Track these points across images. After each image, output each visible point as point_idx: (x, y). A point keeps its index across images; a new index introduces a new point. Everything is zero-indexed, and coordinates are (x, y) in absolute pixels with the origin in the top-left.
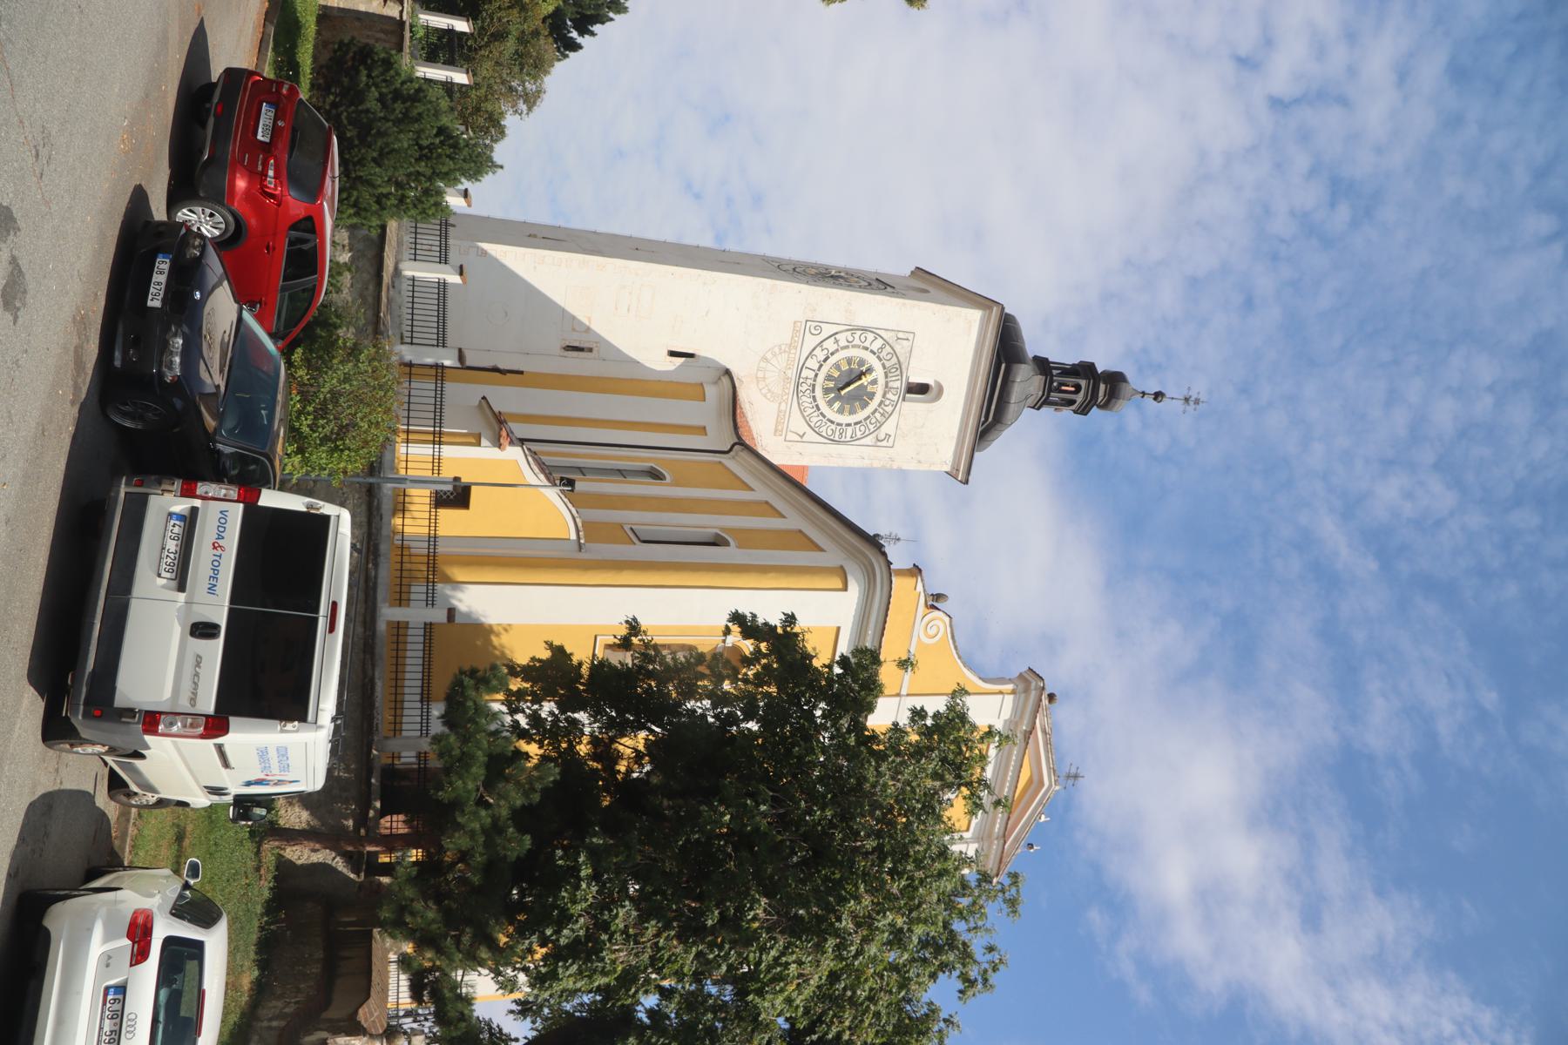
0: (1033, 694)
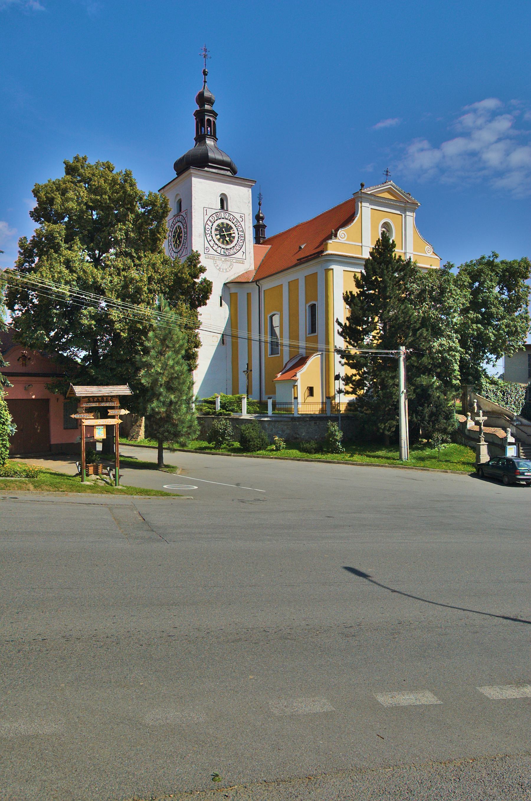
0: (362, 195)
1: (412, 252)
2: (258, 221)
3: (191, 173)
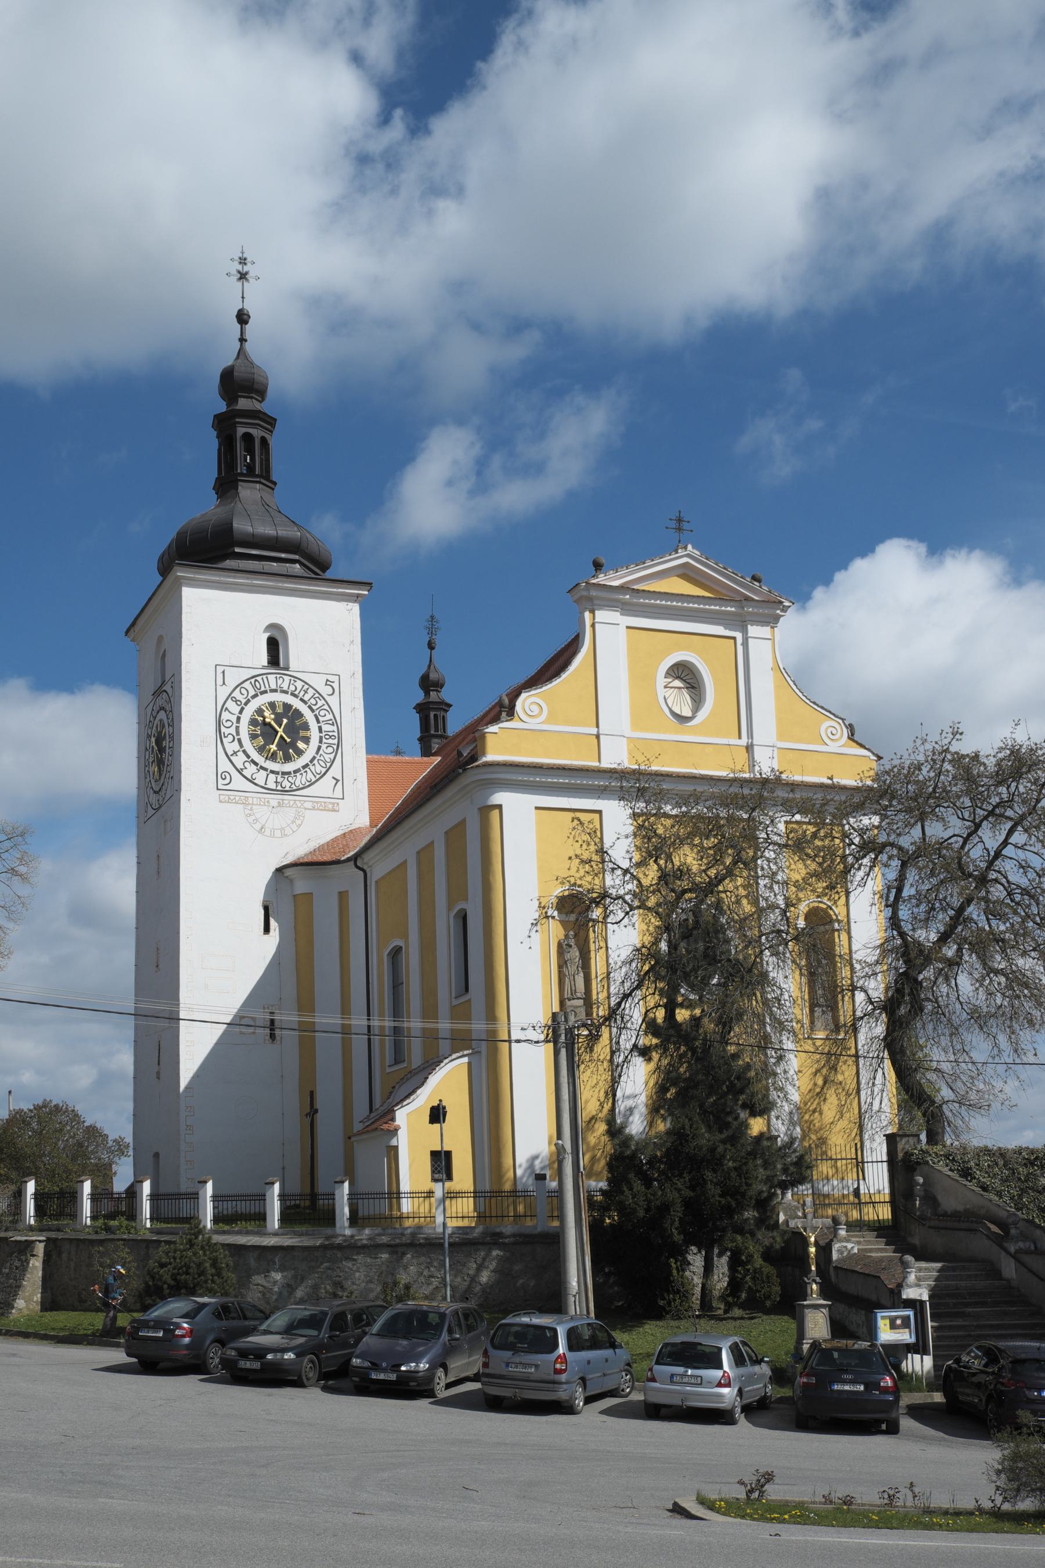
0: (594, 593)
1: (772, 739)
2: (427, 693)
3: (179, 578)
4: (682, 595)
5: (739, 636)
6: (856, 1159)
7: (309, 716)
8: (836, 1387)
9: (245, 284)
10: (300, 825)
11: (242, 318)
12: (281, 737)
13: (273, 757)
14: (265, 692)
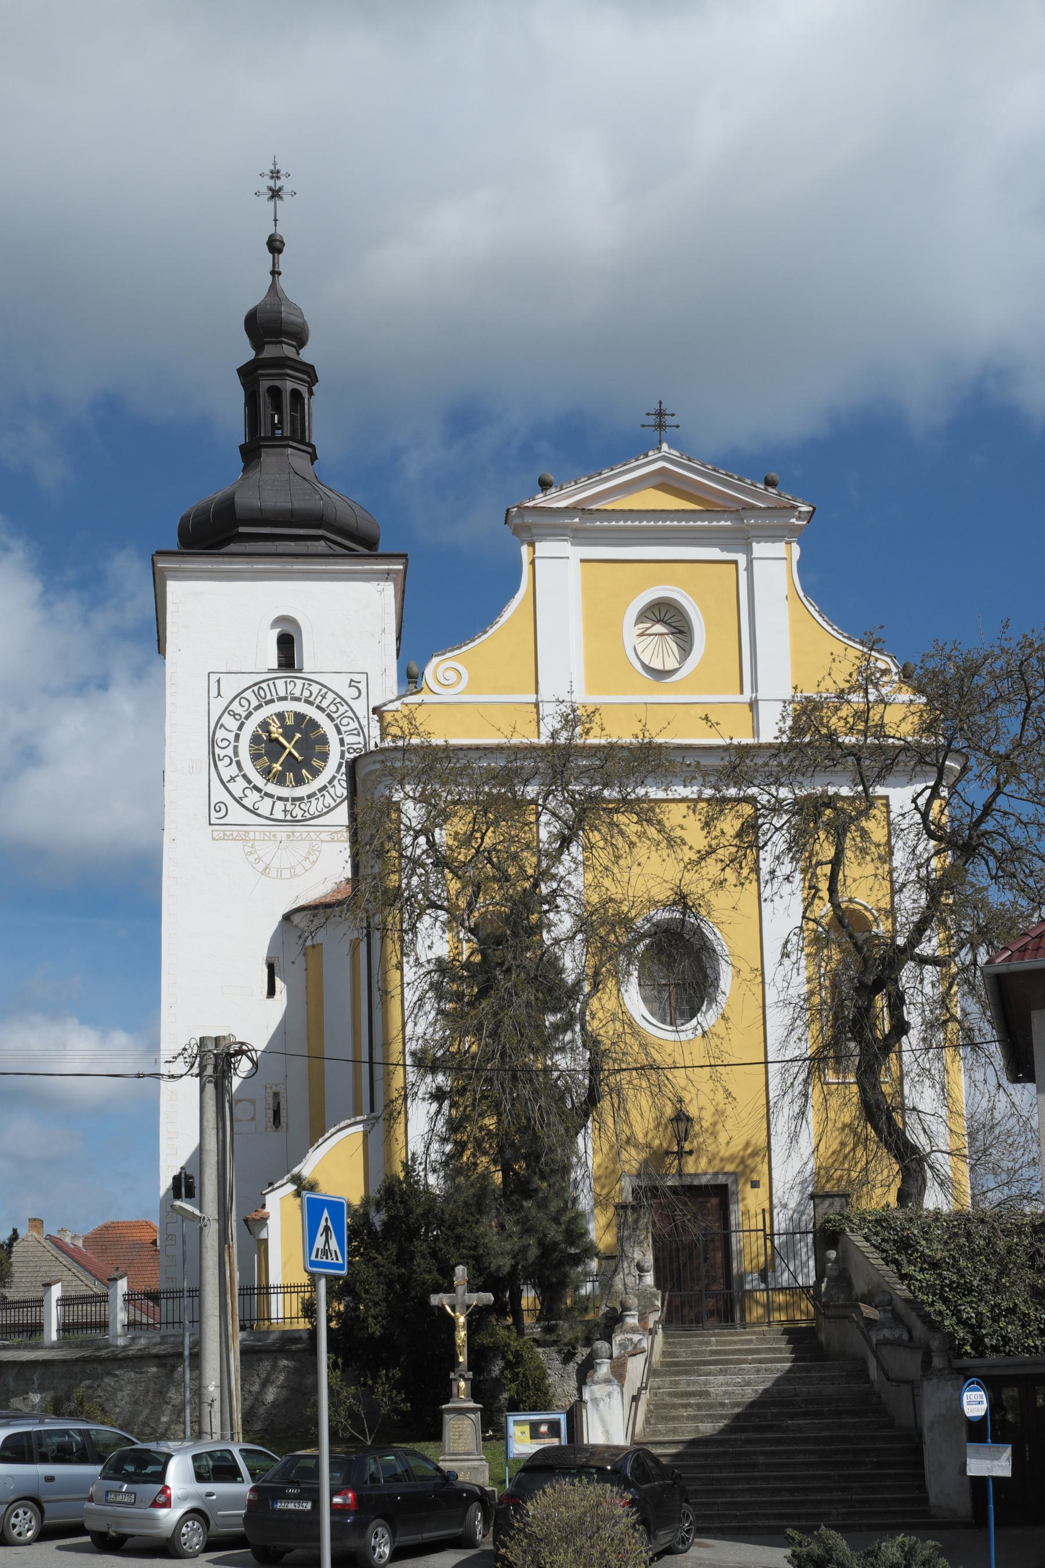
0: (529, 520)
4: (654, 511)
5: (741, 558)
6: (764, 1230)
7: (327, 727)
8: (280, 1505)
9: (279, 202)
10: (315, 862)
11: (275, 246)
12: (290, 753)
13: (280, 780)
14: (272, 701)
